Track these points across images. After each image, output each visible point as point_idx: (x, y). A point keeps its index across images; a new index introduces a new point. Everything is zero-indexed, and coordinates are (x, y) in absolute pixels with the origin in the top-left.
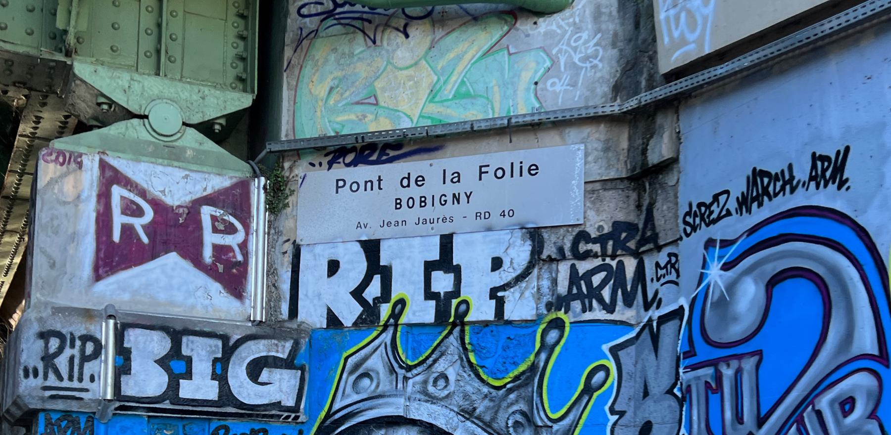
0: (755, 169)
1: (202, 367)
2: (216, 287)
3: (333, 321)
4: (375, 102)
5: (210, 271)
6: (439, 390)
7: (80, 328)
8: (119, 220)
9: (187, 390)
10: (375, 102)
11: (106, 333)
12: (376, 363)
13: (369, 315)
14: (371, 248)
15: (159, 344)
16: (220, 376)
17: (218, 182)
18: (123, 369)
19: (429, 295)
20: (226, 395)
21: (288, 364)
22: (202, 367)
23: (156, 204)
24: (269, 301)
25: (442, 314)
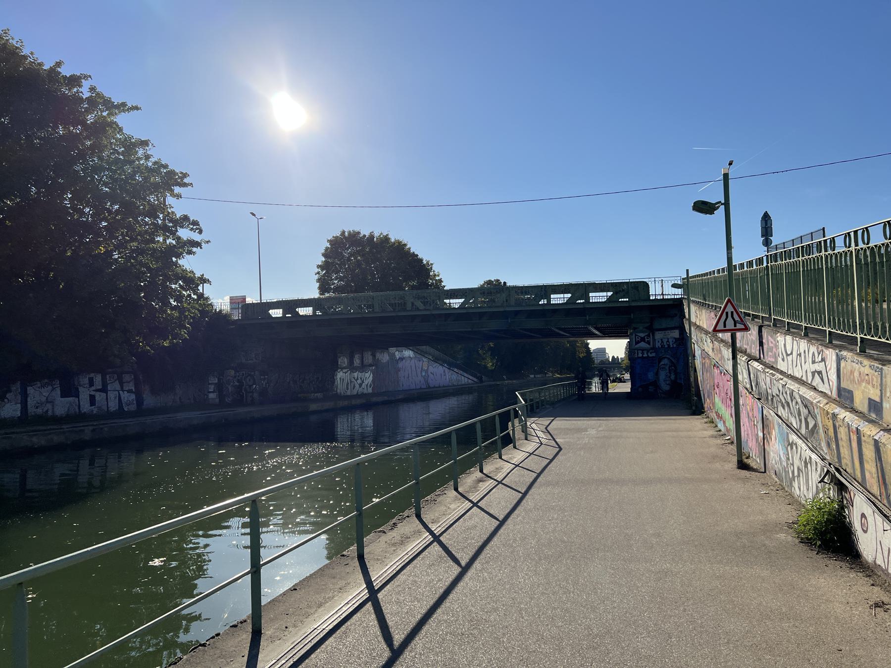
0: (201, 248)
1: (645, 353)
2: (647, 344)
3: (659, 347)
4: (717, 329)
5: (647, 343)
6: (665, 358)
7: (633, 351)
8: (637, 339)
9: (644, 356)
10: (717, 329)
11: (636, 351)
12: (663, 351)
13: (662, 346)
14: (661, 340)
15: (640, 352)
16: (647, 354)
17: (647, 334)
18: (638, 354)
19: (667, 344)
20: (648, 356)
21: (654, 352)
22: (645, 353)
23: (641, 337)
24: (393, 452)
25: (668, 346)
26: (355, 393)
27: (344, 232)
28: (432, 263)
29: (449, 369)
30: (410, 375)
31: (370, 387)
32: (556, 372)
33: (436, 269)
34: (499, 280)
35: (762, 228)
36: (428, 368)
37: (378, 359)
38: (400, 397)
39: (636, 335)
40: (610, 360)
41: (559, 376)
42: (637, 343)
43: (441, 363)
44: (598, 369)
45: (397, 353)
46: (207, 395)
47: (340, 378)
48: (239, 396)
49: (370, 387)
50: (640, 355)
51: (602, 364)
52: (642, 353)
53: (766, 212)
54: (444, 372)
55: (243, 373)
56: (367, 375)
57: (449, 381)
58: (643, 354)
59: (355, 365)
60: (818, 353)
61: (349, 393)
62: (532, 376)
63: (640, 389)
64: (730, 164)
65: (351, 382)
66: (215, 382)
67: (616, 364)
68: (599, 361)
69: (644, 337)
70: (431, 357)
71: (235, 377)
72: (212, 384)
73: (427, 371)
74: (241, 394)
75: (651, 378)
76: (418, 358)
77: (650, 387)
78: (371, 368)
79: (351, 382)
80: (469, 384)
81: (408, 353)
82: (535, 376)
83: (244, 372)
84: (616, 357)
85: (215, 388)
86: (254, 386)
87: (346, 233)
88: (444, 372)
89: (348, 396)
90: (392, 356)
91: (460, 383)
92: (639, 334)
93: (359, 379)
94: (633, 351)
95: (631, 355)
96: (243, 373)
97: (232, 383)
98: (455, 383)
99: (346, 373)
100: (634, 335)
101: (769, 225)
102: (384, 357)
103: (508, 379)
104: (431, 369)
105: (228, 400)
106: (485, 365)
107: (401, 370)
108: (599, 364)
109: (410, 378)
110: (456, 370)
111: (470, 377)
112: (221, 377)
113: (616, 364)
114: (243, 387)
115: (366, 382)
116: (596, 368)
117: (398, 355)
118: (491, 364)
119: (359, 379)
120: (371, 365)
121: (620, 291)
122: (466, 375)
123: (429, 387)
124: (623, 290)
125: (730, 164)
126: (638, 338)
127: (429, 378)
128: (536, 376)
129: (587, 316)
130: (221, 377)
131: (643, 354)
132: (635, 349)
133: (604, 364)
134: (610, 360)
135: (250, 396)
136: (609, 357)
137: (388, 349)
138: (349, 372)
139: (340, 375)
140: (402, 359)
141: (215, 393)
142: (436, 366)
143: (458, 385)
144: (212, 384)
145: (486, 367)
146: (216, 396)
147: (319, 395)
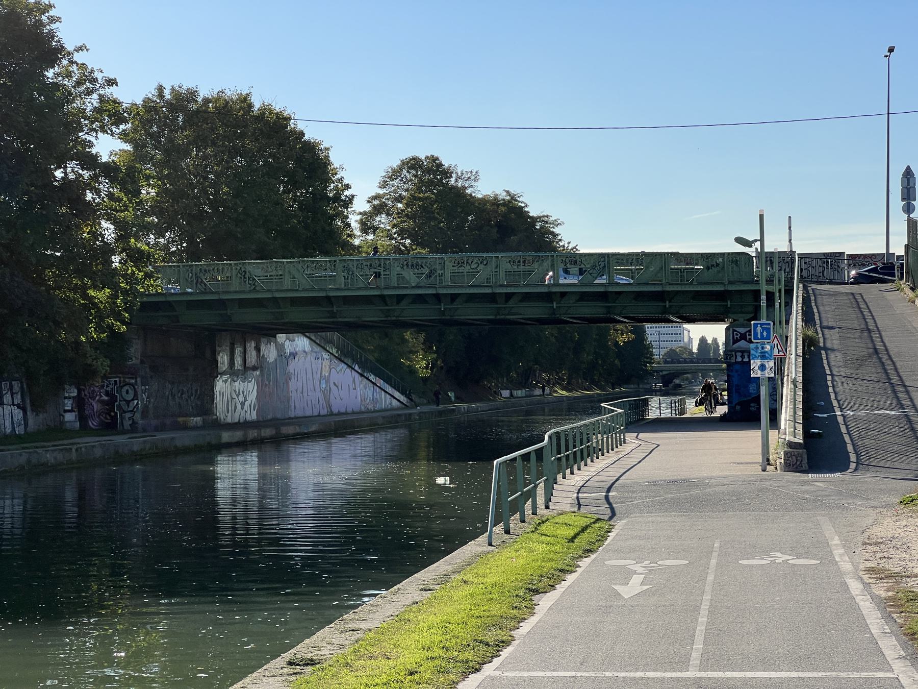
9: (744, 360)
11: (734, 353)
15: (739, 354)
18: (736, 358)
26: (236, 420)
27: (160, 89)
28: (327, 146)
29: (362, 375)
30: (305, 389)
31: (254, 410)
32: (558, 382)
33: (335, 159)
34: (437, 159)
35: (903, 188)
36: (330, 374)
37: (263, 355)
38: (313, 428)
39: (734, 331)
40: (695, 350)
41: (564, 393)
42: (735, 342)
43: (349, 362)
44: (663, 376)
45: (287, 343)
46: (63, 416)
47: (220, 391)
48: (108, 417)
49: (254, 410)
50: (739, 359)
51: (672, 362)
52: (741, 357)
53: (909, 166)
54: (354, 381)
55: (116, 382)
56: (251, 385)
57: (361, 400)
58: (743, 357)
59: (236, 368)
60: (404, 408)
61: (229, 420)
62: (506, 393)
63: (738, 408)
64: (891, 50)
65: (232, 398)
66: (72, 395)
67: (710, 361)
68: (663, 352)
69: (745, 333)
70: (334, 351)
71: (103, 387)
72: (69, 398)
73: (328, 380)
74: (113, 414)
75: (753, 392)
76: (316, 352)
77: (752, 405)
78: (255, 373)
79: (232, 398)
80: (392, 409)
81: (301, 343)
82: (511, 395)
83: (117, 379)
84: (710, 341)
85: (74, 406)
86: (136, 401)
87: (347, 193)
88: (354, 381)
89: (229, 424)
90: (280, 348)
91: (378, 407)
92: (737, 329)
93: (241, 393)
94: (730, 353)
95: (727, 358)
96: (116, 382)
97: (97, 398)
98: (370, 407)
99: (226, 381)
100: (731, 329)
101: (911, 185)
102: (270, 352)
103: (459, 399)
104: (335, 377)
105: (93, 424)
106: (409, 366)
107: (293, 377)
108: (666, 362)
109: (305, 394)
110: (372, 377)
111: (397, 394)
112: (83, 387)
113: (710, 361)
114: (116, 404)
115: (249, 399)
116: (657, 372)
117: (288, 348)
118: (424, 364)
119: (241, 393)
120: (254, 368)
121: (713, 266)
122: (389, 389)
123: (332, 414)
124: (718, 265)
125: (891, 50)
126: (737, 335)
127: (332, 394)
128: (515, 393)
129: (667, 302)
130: (83, 387)
131: (743, 357)
132: (732, 351)
133: (680, 362)
134: (695, 350)
135: (129, 419)
136: (690, 340)
137: (275, 337)
138: (229, 380)
139: (221, 385)
140: (294, 355)
141: (74, 413)
142: (341, 370)
143: (375, 411)
144: (69, 398)
145: (412, 371)
146: (74, 418)
147: (198, 420)
